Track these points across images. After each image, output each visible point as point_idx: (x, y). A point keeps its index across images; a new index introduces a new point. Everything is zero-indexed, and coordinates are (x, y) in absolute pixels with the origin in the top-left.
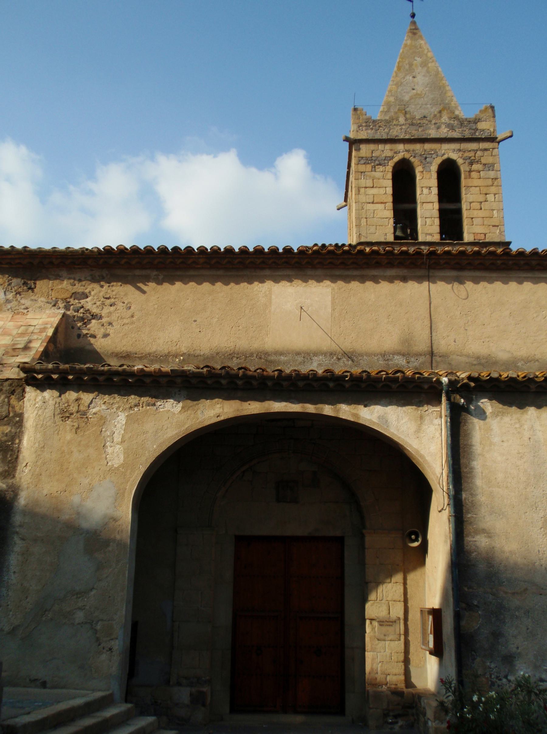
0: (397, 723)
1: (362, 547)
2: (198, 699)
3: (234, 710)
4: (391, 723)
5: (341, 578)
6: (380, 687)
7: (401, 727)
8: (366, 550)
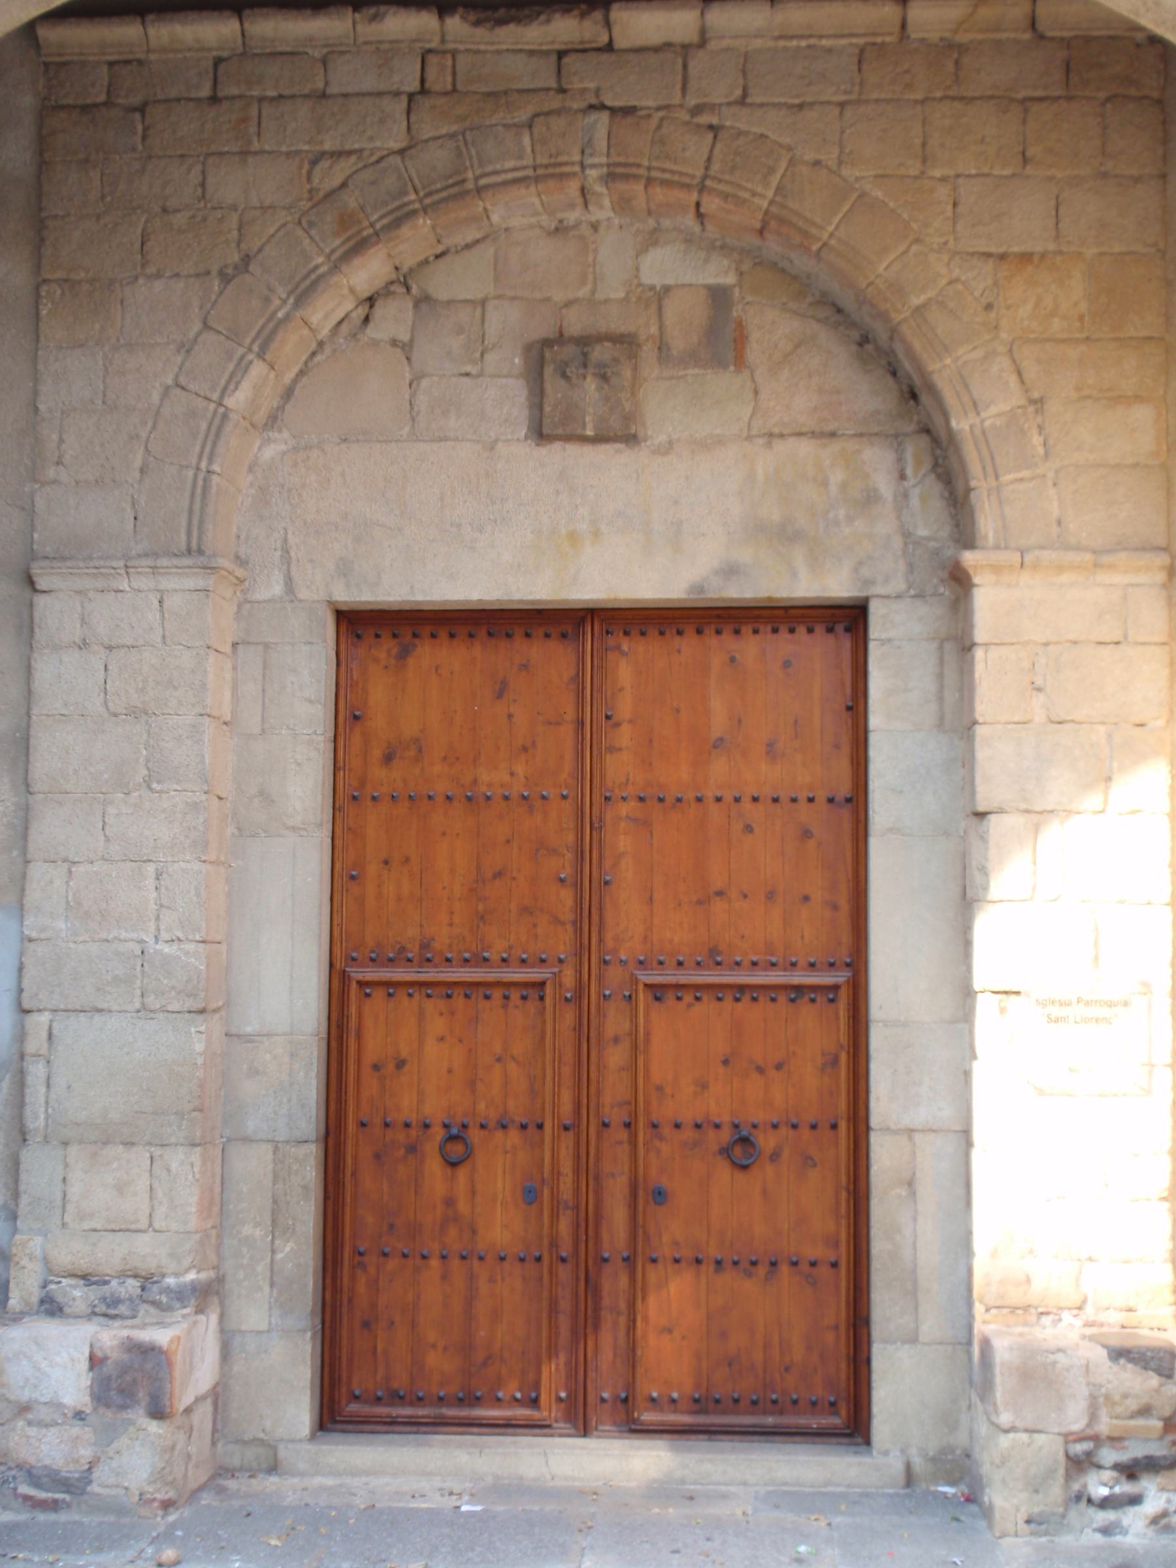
0: (1135, 1500)
1: (958, 644)
2: (131, 1384)
3: (335, 1412)
4: (1105, 1503)
5: (856, 801)
6: (1046, 1320)
7: (1158, 1520)
8: (979, 653)
